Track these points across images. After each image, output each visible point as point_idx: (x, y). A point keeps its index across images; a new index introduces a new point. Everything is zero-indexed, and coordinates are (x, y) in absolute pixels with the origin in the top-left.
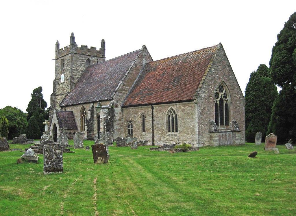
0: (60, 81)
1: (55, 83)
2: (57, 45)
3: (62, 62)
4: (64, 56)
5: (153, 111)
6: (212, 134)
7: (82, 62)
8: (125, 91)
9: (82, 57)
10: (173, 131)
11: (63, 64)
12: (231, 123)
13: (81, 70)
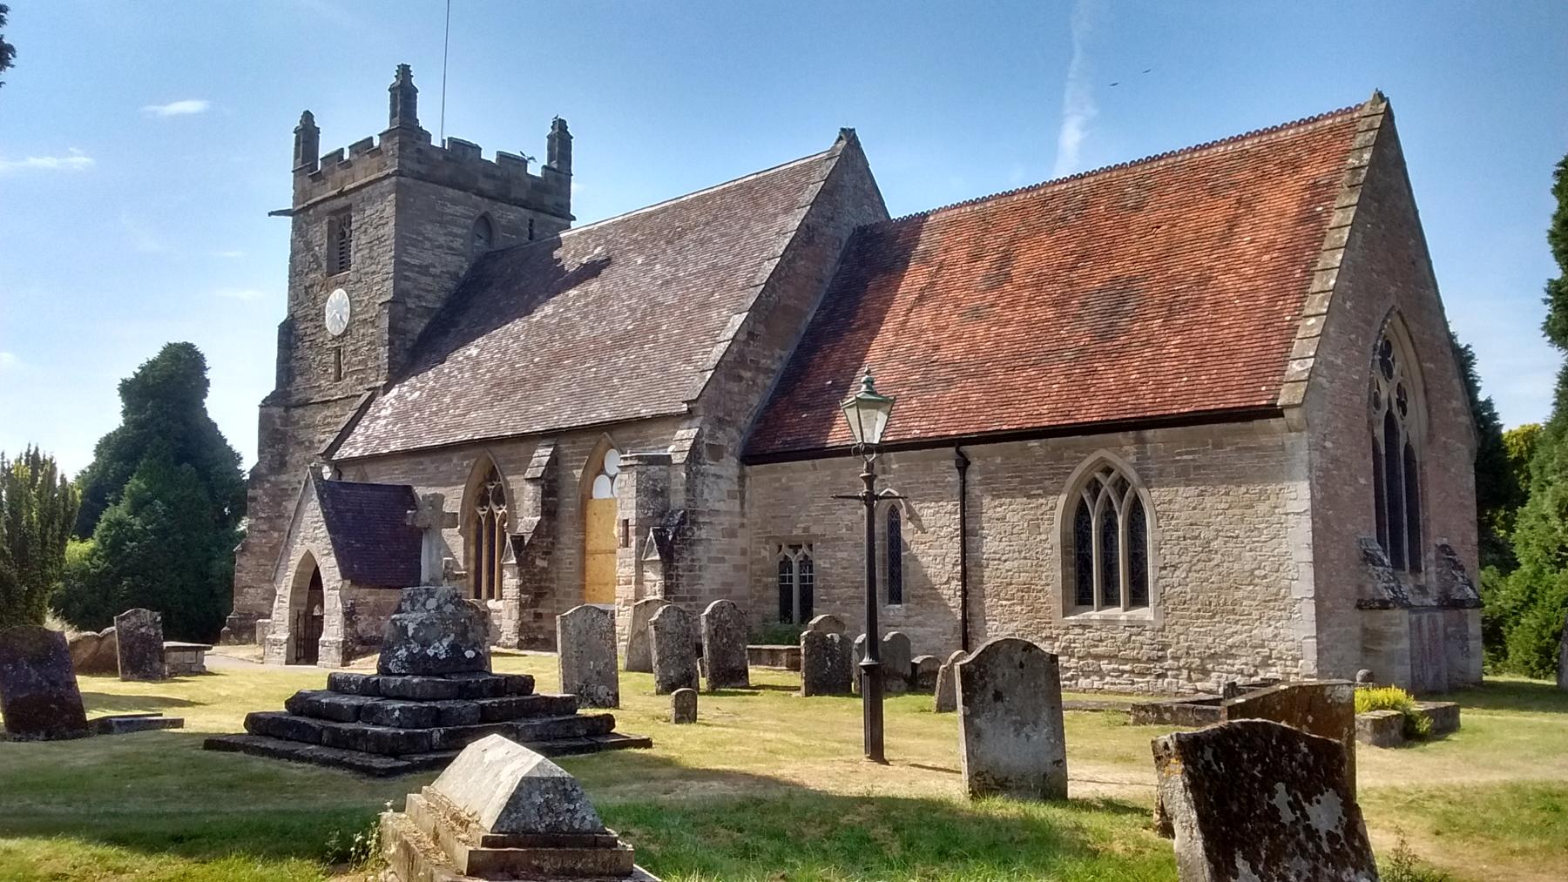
0: (321, 328)
1: (289, 336)
2: (307, 134)
3: (337, 226)
4: (351, 191)
5: (964, 483)
6: (1379, 619)
7: (455, 230)
8: (758, 369)
9: (454, 202)
10: (1110, 600)
11: (343, 234)
12: (1431, 555)
13: (448, 272)
